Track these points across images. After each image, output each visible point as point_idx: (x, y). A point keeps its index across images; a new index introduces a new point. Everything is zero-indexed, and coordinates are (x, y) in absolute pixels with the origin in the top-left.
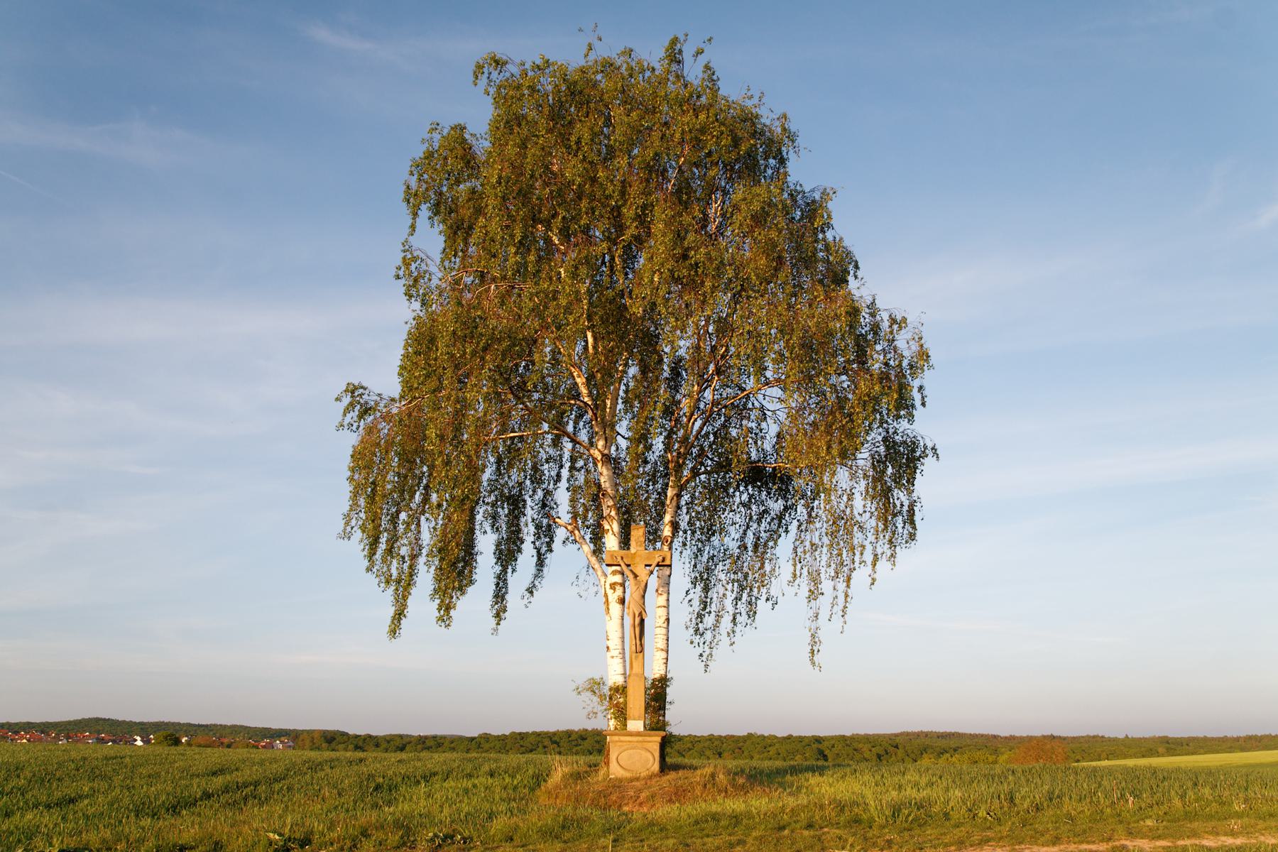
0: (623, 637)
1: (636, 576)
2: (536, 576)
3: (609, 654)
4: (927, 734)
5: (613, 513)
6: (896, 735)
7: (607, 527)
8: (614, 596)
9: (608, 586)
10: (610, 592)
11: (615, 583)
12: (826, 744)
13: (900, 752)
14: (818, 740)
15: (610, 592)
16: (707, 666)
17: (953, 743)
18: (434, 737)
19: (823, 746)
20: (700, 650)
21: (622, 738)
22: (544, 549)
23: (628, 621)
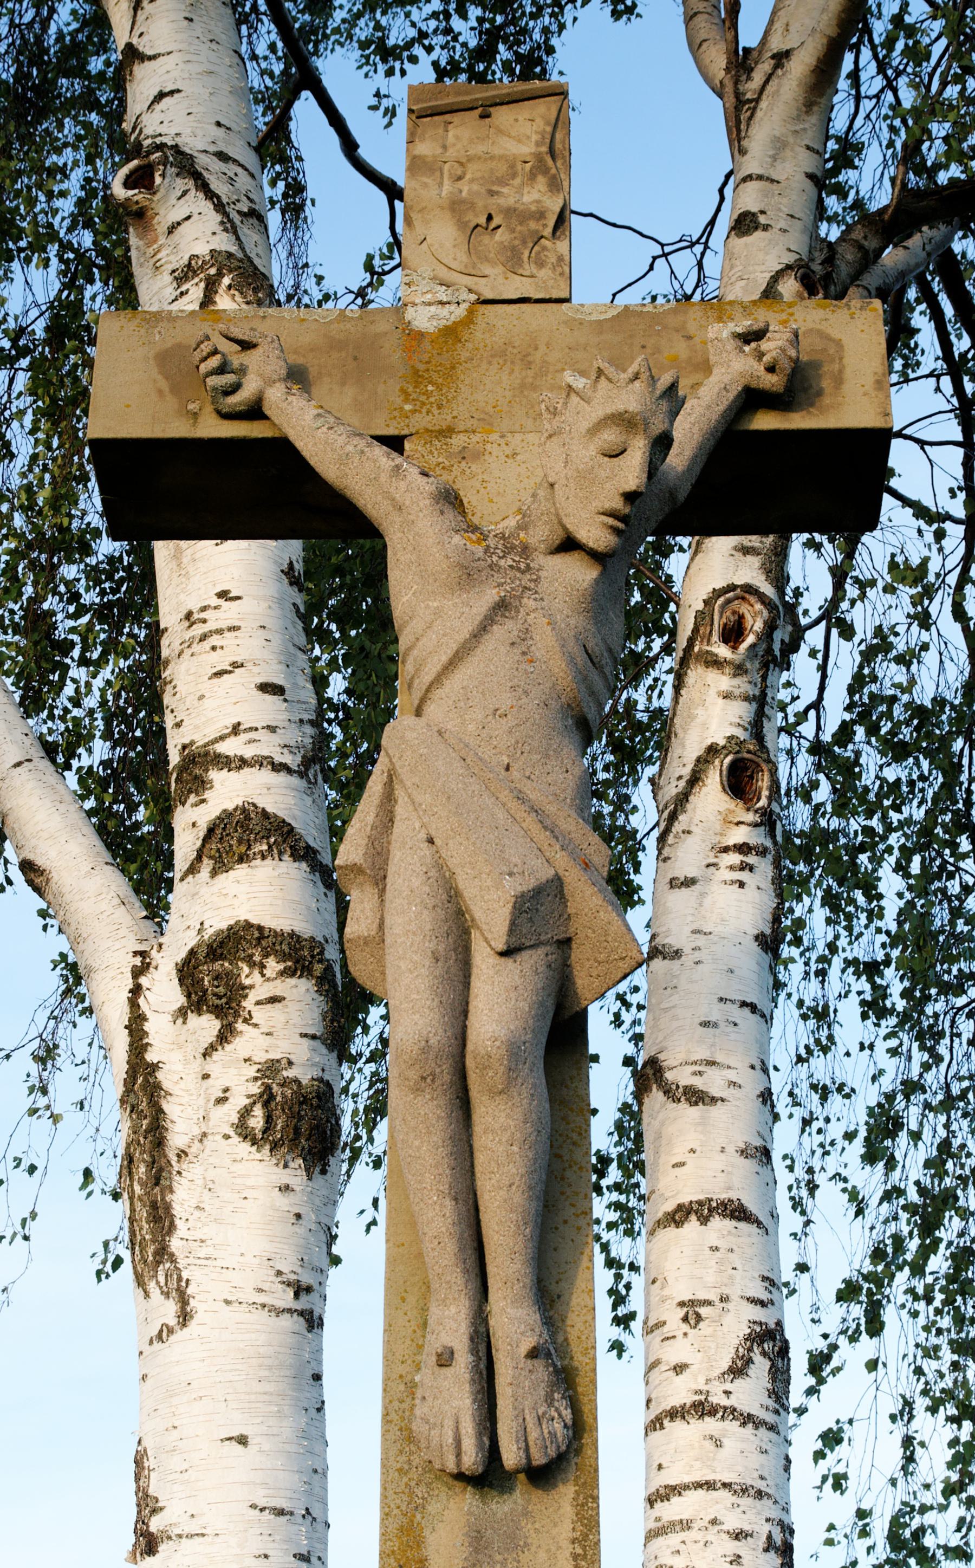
9: (164, 991)
10: (177, 1043)
11: (237, 942)
15: (177, 1043)
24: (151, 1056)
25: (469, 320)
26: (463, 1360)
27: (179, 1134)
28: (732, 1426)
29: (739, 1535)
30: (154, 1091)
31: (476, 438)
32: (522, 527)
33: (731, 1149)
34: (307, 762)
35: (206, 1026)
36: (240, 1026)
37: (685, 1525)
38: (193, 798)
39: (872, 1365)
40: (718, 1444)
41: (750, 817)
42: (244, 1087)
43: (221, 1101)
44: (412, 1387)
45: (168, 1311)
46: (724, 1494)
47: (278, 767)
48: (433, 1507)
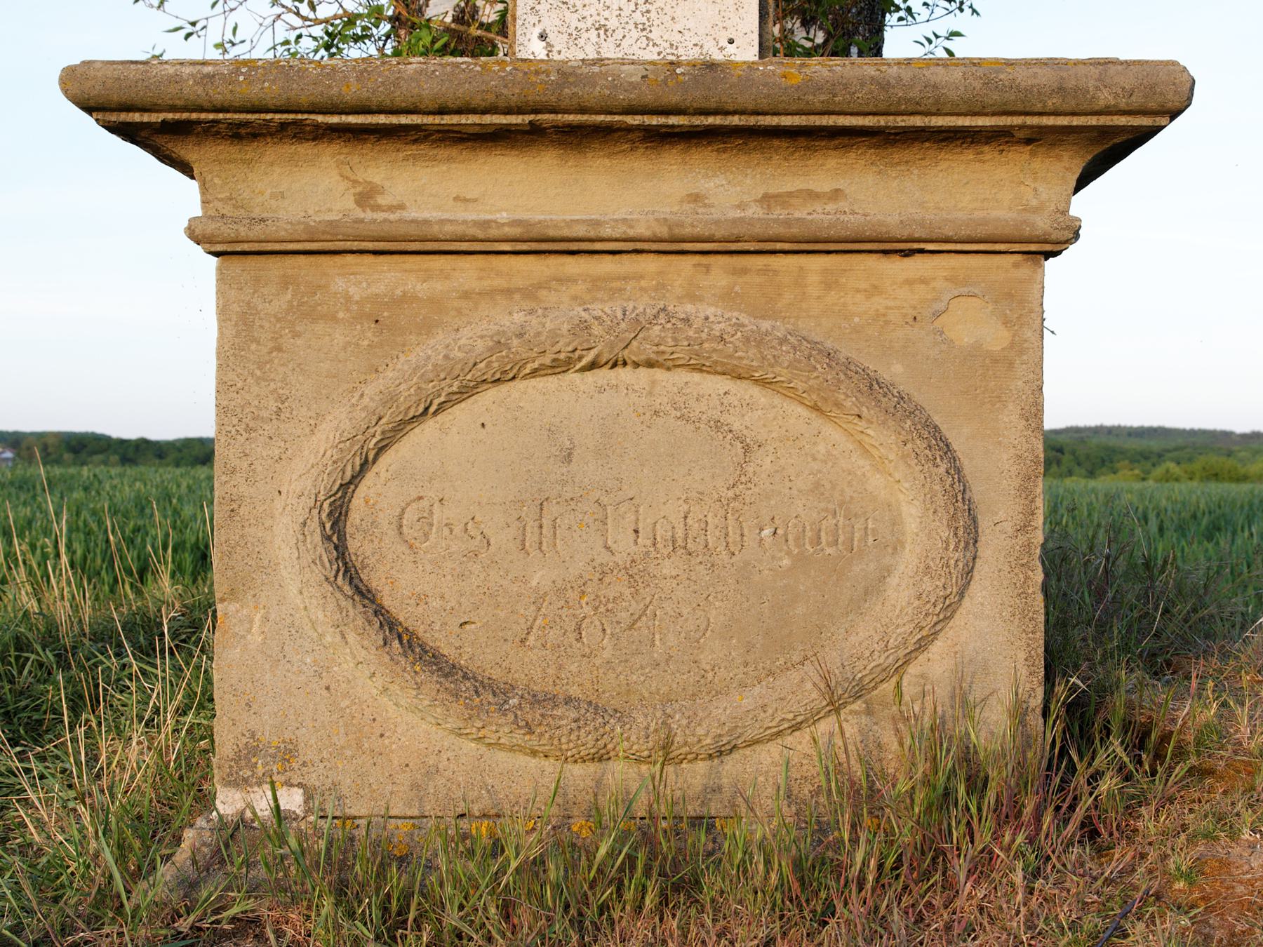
17: (1155, 445)
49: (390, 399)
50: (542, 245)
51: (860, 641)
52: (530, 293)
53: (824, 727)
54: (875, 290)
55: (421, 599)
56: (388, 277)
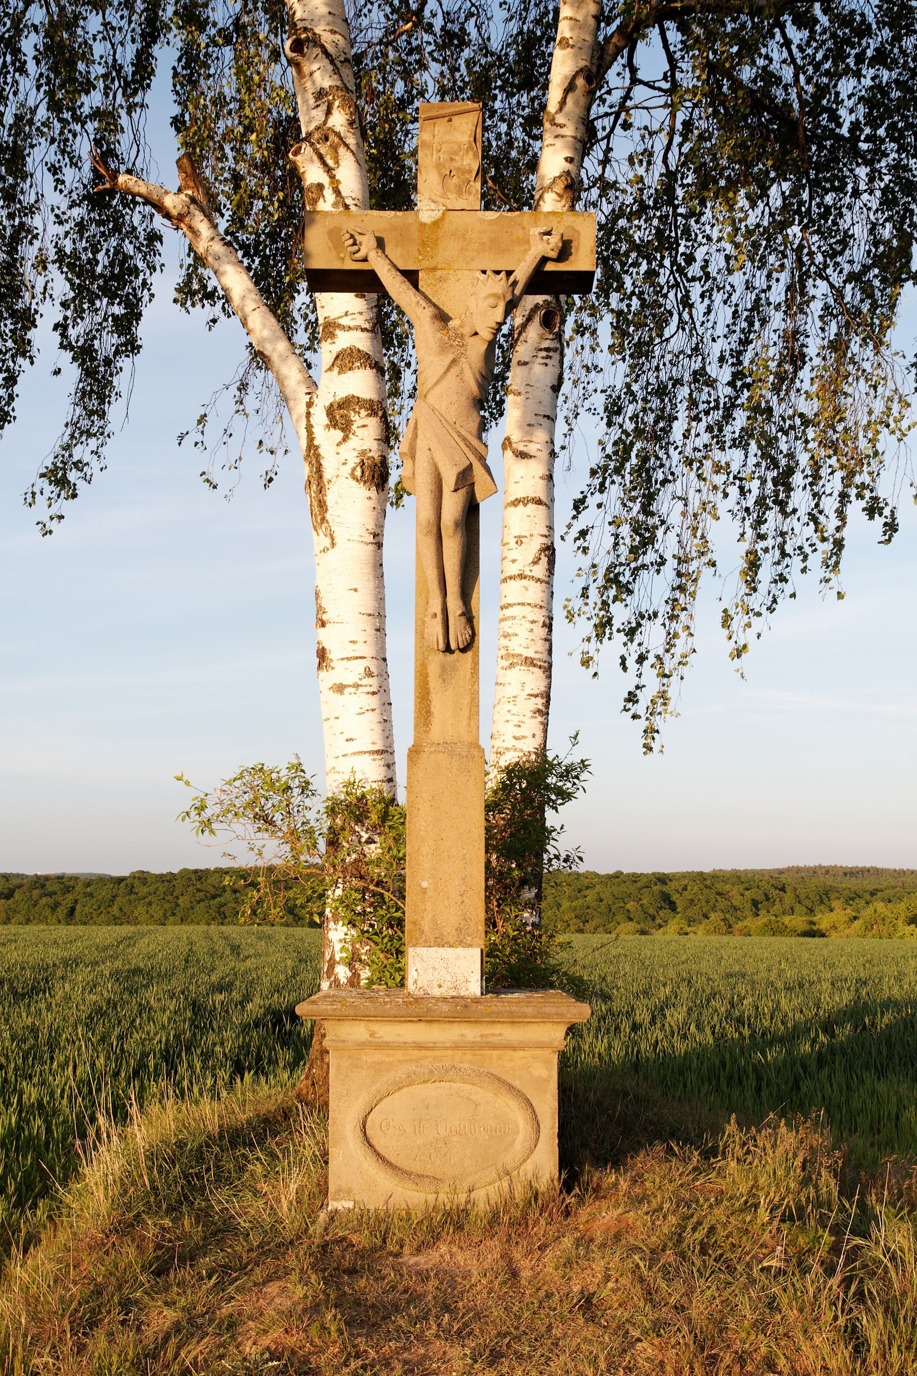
0: (379, 614)
1: (442, 317)
2: (79, 432)
3: (328, 678)
4: (827, 871)
5: (339, 120)
6: (781, 872)
7: (313, 174)
8: (342, 455)
9: (320, 418)
10: (327, 438)
11: (347, 403)
12: (673, 885)
13: (788, 898)
14: (662, 879)
15: (327, 438)
16: (651, 731)
17: (868, 884)
18: (60, 878)
19: (670, 888)
20: (629, 682)
21: (388, 1032)
22: (107, 343)
23: (406, 527)
24: (316, 443)
25: (442, 218)
26: (440, 616)
27: (328, 474)
28: (532, 583)
29: (533, 622)
30: (318, 457)
31: (445, 272)
32: (461, 326)
33: (537, 477)
34: (375, 325)
35: (338, 434)
36: (351, 436)
37: (514, 618)
38: (329, 340)
39: (599, 506)
40: (527, 589)
41: (551, 336)
42: (354, 461)
43: (344, 464)
44: (424, 622)
45: (327, 542)
46: (528, 607)
47: (363, 330)
48: (430, 658)
49: (379, 1091)
50: (419, 1046)
51: (509, 1159)
52: (417, 1061)
53: (496, 1185)
54: (511, 1060)
55: (387, 1147)
56: (378, 1056)
